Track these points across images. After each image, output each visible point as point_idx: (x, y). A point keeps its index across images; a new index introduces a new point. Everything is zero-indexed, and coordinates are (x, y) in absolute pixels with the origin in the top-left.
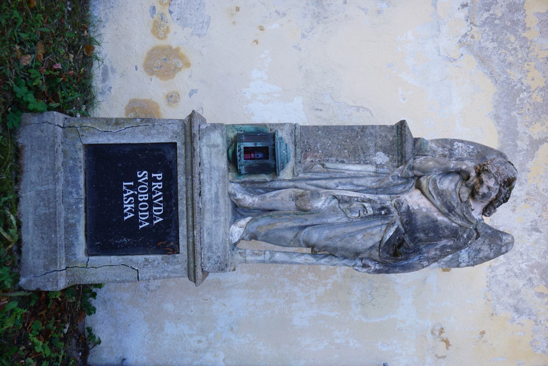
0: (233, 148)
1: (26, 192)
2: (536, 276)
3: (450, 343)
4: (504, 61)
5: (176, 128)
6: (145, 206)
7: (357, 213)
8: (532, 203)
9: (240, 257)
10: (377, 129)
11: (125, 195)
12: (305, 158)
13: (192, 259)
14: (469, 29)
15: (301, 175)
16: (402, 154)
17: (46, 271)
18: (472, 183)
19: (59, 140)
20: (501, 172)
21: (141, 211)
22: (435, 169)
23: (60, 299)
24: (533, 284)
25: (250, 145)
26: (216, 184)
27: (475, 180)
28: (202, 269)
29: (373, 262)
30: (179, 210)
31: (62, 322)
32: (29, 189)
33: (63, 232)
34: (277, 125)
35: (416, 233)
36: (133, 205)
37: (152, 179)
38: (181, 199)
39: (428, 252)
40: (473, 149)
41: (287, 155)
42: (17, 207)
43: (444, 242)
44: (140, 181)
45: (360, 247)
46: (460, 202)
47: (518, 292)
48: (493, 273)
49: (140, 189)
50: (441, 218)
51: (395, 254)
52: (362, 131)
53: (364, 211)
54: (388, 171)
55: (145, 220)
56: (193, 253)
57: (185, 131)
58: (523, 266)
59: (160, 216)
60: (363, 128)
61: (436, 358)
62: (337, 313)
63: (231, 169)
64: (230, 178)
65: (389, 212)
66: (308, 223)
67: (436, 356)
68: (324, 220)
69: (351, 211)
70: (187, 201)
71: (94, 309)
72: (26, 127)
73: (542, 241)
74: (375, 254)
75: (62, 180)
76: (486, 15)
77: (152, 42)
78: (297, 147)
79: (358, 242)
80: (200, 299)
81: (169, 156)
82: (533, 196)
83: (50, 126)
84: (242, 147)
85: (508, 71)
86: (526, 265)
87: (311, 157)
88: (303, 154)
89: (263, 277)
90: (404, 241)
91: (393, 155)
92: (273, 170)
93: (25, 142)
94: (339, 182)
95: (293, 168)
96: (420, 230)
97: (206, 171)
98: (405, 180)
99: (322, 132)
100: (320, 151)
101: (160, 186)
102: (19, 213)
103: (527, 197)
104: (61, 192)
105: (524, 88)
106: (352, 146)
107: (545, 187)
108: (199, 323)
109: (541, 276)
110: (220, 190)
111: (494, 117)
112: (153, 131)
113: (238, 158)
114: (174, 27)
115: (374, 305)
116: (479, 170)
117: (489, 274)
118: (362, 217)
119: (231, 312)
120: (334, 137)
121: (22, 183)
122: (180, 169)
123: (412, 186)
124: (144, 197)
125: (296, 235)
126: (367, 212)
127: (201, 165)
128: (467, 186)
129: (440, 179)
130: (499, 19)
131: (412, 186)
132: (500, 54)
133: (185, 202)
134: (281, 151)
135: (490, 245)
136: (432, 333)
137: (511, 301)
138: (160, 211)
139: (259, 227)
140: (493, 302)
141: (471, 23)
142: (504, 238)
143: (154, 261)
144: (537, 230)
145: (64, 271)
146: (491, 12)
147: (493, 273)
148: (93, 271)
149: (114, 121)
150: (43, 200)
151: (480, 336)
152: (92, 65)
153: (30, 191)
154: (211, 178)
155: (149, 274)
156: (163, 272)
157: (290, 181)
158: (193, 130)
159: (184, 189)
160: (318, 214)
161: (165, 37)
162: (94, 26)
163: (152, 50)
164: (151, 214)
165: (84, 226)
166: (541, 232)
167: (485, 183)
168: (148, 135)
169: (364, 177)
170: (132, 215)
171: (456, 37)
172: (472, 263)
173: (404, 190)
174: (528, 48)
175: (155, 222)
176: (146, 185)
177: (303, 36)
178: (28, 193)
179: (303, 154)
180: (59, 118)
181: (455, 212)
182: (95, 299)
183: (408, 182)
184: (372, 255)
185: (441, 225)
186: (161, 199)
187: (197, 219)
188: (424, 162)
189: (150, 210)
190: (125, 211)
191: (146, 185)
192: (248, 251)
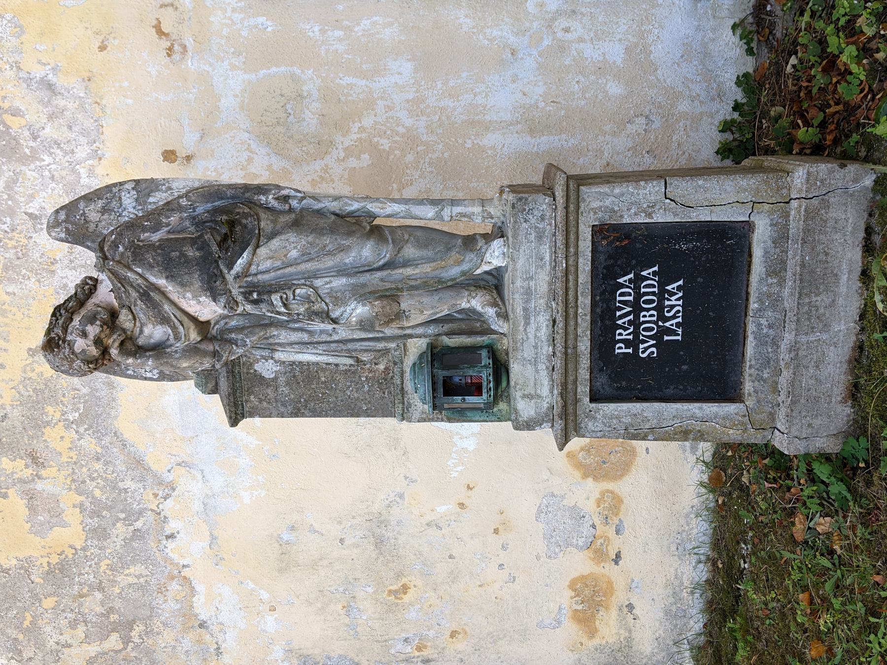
0: (499, 390)
1: (847, 329)
2: (27, 145)
3: (154, 30)
4: (106, 463)
5: (590, 424)
6: (645, 302)
7: (299, 295)
8: (45, 258)
9: (492, 210)
10: (274, 412)
11: (680, 320)
12: (386, 369)
13: (571, 218)
14: (161, 506)
15: (393, 345)
16: (234, 376)
17: (826, 197)
18: (115, 336)
19: (782, 412)
20: (65, 362)
21: (653, 293)
22: (177, 355)
23: (799, 121)
24: (29, 130)
25: (471, 399)
26: (528, 338)
27: (110, 341)
28: (554, 200)
29: (270, 206)
30: (590, 297)
31: (798, 79)
32: (841, 334)
33: (790, 264)
34: (432, 420)
35: (201, 257)
36: (667, 303)
37: (635, 343)
38: (585, 315)
39: (181, 218)
40: (128, 370)
41: (415, 378)
42: (866, 305)
43: (156, 237)
44: (652, 342)
45: (292, 236)
46: (132, 307)
47: (51, 117)
48: (94, 147)
49: (653, 329)
50: (161, 282)
51: (232, 224)
52: (299, 410)
53: (287, 299)
54: (254, 352)
55: (647, 279)
56: (569, 229)
57: (575, 421)
58: (48, 159)
59: (622, 286)
60: (296, 413)
61: (176, 3)
62: (341, 82)
63: (504, 354)
64: (505, 341)
65: (247, 295)
66: (379, 274)
67: (177, 8)
68: (352, 281)
69: (307, 299)
70: (576, 313)
71: (738, 83)
72: (835, 432)
73: (23, 199)
74: (266, 224)
75: (784, 346)
76: (139, 524)
77: (623, 487)
78: (400, 387)
79: (295, 245)
80: (563, 102)
81: (603, 379)
82: (44, 269)
83: (796, 434)
84: (485, 396)
85: (99, 450)
86: (44, 160)
87: (377, 370)
88: (391, 375)
89: (460, 141)
90: (219, 246)
91: (247, 373)
92: (436, 355)
93: (839, 408)
94: (331, 335)
95: (405, 354)
96: (194, 263)
97: (543, 358)
98: (226, 336)
99: (361, 408)
100: (364, 379)
101: (620, 334)
102: (862, 295)
103: (53, 268)
104: (786, 329)
105: (74, 427)
106: (313, 386)
107: (27, 282)
108: (567, 63)
109: (18, 143)
110: (521, 328)
111: (115, 385)
112: (627, 420)
113: (491, 378)
114: (589, 506)
115: (282, 95)
116: (104, 358)
117: (101, 146)
118: (289, 288)
119: (514, 81)
120: (342, 401)
121: (851, 344)
122: (585, 362)
123: (215, 324)
124: (648, 316)
125: (398, 252)
126: (281, 297)
127: (551, 368)
128: (124, 331)
129: (168, 339)
130: (120, 519)
131: (215, 324)
132: (113, 472)
133: (580, 310)
134: (425, 387)
135: (86, 222)
136: (184, 47)
137: (61, 102)
138: (622, 295)
139: (459, 263)
140: (90, 101)
141: (159, 514)
142: (63, 235)
143: (636, 214)
144: (31, 215)
145: (793, 196)
146: (132, 528)
147: (94, 147)
148: (743, 197)
149: (691, 436)
150: (818, 317)
151: (106, 43)
152: (714, 455)
153: (840, 331)
154: (536, 347)
155: (647, 191)
156: (623, 195)
157: (411, 336)
158: (563, 425)
159: (579, 330)
160: (361, 292)
161: (603, 494)
162: (707, 509)
163: (622, 475)
164: (637, 289)
165: (753, 272)
166: (26, 213)
167: (90, 343)
168: (635, 415)
169: (291, 344)
170: (669, 288)
171: (179, 496)
172: (115, 190)
173: (227, 320)
174: (73, 480)
175: (631, 276)
176: (643, 336)
177: (401, 496)
178: (843, 327)
179: (391, 375)
180: (781, 443)
181: (138, 292)
182: (736, 101)
183: (222, 331)
184: (272, 221)
185: (159, 271)
186: (618, 313)
187: (559, 286)
188: (197, 365)
189: (638, 295)
190: (680, 294)
191: (643, 336)
192: (479, 220)
